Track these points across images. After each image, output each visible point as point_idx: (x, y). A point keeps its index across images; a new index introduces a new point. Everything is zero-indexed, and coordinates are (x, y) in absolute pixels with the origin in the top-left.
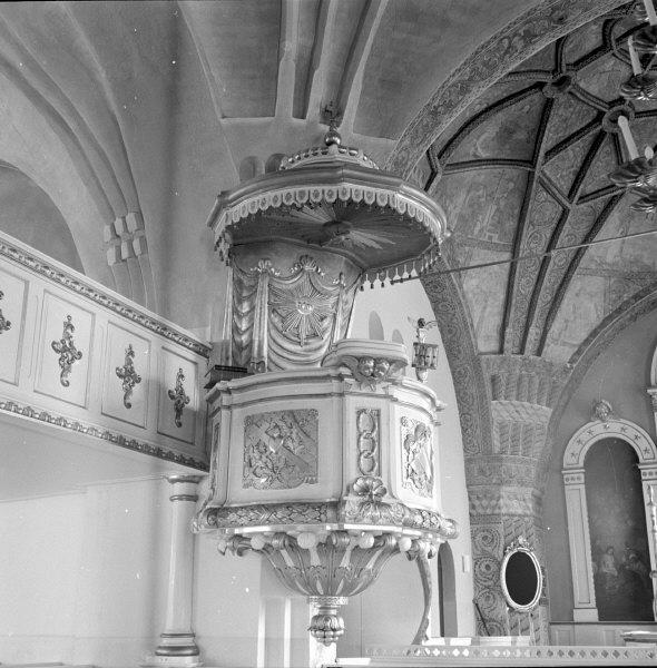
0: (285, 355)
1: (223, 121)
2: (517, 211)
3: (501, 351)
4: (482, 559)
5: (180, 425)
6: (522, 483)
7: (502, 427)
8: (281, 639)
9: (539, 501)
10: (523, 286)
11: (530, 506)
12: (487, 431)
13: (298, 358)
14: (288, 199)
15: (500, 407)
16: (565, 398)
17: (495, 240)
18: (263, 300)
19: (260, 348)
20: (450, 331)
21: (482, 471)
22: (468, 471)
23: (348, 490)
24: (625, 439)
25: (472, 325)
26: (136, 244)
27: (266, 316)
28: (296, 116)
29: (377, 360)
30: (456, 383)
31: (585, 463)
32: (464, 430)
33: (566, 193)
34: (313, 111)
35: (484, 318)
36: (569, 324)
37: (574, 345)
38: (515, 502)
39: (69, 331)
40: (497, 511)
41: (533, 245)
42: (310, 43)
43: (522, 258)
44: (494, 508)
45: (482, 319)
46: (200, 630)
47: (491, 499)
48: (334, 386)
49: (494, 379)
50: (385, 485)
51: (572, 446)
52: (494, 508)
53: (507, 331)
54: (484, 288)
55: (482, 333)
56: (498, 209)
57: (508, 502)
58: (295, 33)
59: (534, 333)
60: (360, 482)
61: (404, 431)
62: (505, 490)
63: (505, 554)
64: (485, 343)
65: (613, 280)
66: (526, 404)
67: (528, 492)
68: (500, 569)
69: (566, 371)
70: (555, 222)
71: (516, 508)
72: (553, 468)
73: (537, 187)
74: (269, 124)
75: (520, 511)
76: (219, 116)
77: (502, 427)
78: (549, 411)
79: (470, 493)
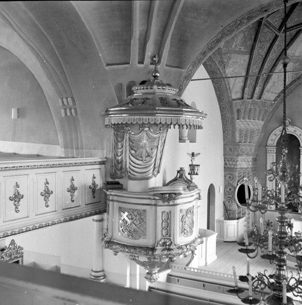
0: (136, 166)
1: (107, 68)
2: (253, 37)
3: (242, 98)
4: (228, 186)
5: (94, 197)
6: (247, 155)
7: (241, 131)
8: (136, 275)
9: (255, 160)
10: (254, 69)
11: (250, 163)
12: (234, 133)
13: (139, 167)
14: (134, 121)
15: (240, 123)
16: (271, 115)
17: (242, 50)
18: (126, 143)
19: (126, 164)
20: (219, 91)
21: (230, 149)
22: (224, 149)
23: (158, 244)
24: (295, 135)
25: (230, 88)
26: (73, 111)
27: (128, 152)
28: (139, 63)
29: (170, 194)
30: (221, 111)
31: (277, 143)
32: (224, 132)
33: (278, 28)
34: (147, 60)
35: (235, 87)
36: (275, 84)
37: (276, 93)
38: (244, 163)
39: (47, 185)
40: (236, 167)
41: (260, 52)
42: (145, 29)
43: (251, 76)
44: (235, 165)
45: (234, 84)
46: (105, 270)
47: (234, 161)
48: (153, 202)
49: (238, 111)
50: (172, 240)
51: (272, 137)
52: (235, 165)
53: (246, 89)
54: (236, 71)
55: (234, 90)
56: (244, 36)
57: (241, 163)
58: (138, 25)
59: (258, 89)
60: (163, 241)
61: (181, 214)
62: (240, 158)
63: (237, 185)
64: (236, 94)
65: (297, 64)
66: (252, 121)
67: (250, 158)
68: (235, 191)
69: (272, 105)
70: (272, 40)
71: (244, 165)
72: (263, 146)
73: (263, 27)
74: (126, 68)
75: (246, 166)
76: (105, 65)
77: (241, 131)
78: (262, 123)
79: (225, 159)
